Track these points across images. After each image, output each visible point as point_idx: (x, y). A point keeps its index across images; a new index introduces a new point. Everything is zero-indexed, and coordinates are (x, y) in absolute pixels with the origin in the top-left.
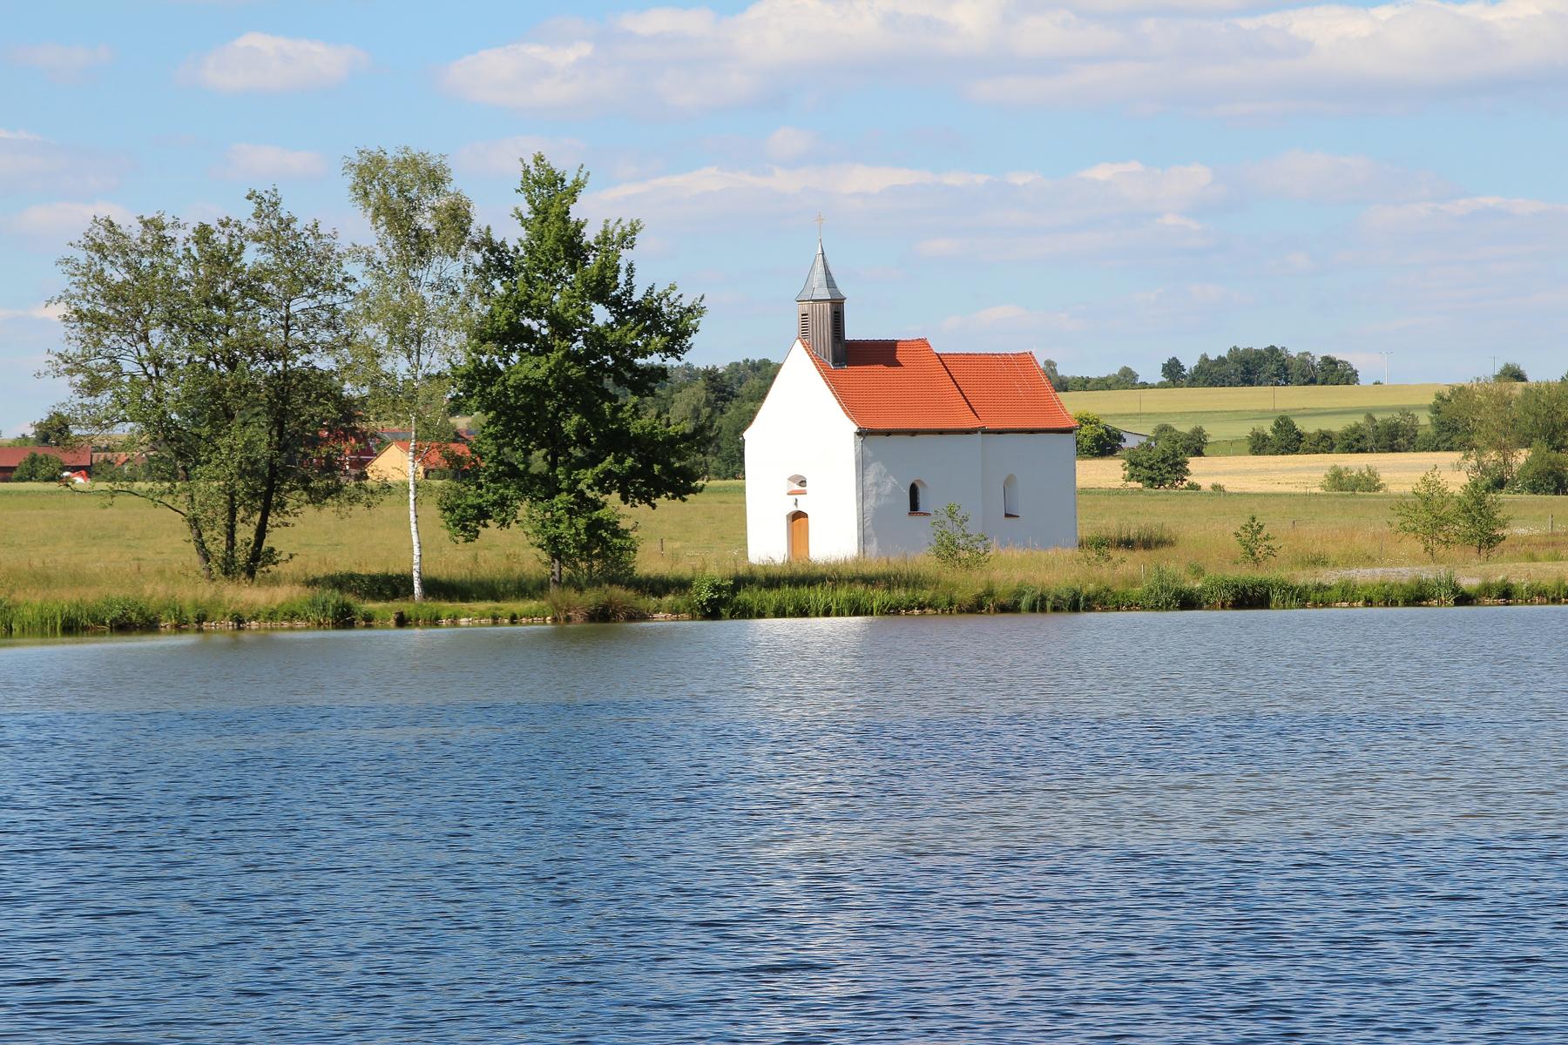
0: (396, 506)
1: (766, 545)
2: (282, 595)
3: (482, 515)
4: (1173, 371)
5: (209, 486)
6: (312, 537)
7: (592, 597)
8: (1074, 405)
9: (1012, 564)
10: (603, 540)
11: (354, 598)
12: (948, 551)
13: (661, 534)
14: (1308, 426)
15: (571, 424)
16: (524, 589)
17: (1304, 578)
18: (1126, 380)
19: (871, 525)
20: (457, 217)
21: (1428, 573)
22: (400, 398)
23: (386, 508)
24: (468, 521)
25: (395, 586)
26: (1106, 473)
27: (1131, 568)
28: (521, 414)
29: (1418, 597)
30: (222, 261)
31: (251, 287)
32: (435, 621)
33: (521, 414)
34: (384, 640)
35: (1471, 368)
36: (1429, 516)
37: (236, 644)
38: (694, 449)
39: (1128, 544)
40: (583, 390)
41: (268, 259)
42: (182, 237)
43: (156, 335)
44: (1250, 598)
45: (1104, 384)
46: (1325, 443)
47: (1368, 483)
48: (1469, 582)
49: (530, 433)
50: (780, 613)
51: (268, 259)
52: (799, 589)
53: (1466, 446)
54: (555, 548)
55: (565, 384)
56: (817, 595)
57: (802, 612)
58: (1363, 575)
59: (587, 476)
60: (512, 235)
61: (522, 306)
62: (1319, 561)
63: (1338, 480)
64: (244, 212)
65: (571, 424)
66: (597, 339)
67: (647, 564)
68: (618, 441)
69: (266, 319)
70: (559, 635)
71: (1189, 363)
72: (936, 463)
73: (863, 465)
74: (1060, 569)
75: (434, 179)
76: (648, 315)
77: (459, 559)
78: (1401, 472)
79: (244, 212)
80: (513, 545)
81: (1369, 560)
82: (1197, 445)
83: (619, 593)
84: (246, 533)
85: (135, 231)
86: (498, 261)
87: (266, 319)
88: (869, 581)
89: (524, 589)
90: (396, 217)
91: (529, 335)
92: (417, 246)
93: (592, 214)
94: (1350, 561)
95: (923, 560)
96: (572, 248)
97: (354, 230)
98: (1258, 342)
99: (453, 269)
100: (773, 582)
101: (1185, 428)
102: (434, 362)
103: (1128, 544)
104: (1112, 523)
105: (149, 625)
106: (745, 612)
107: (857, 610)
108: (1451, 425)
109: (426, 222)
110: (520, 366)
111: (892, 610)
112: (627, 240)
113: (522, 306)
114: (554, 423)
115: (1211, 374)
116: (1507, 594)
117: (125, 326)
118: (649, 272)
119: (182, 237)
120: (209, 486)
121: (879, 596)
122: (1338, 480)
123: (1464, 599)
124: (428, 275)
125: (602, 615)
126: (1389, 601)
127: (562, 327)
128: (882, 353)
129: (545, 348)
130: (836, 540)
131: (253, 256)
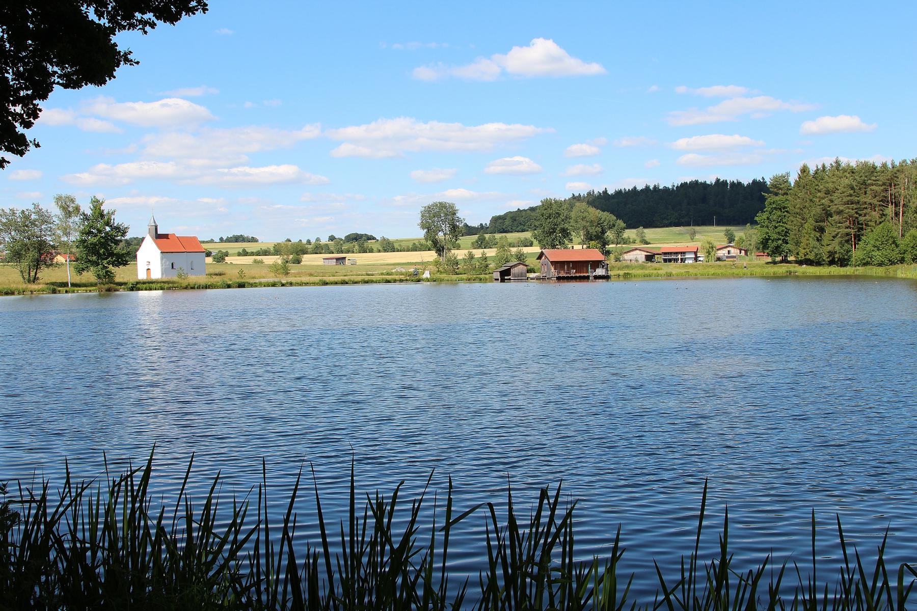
0: (63, 268)
1: (142, 276)
2: (41, 286)
3: (83, 270)
4: (221, 239)
5: (25, 264)
6: (46, 275)
7: (107, 286)
8: (205, 246)
9: (193, 279)
10: (109, 275)
11: (56, 287)
12: (180, 276)
13: (121, 274)
14: (249, 250)
15: (102, 251)
16: (92, 285)
17: (252, 281)
18: (212, 241)
19: (164, 272)
20: (77, 209)
21: (276, 280)
22: (64, 244)
23: (63, 268)
24: (80, 271)
25: (65, 285)
26: (209, 260)
27: (217, 279)
28: (92, 249)
29: (274, 285)
30: (27, 217)
31: (33, 223)
32: (73, 292)
33: (92, 249)
34: (64, 297)
35: (281, 239)
36: (274, 268)
37: (31, 298)
38: (126, 257)
39: (216, 275)
40: (104, 245)
41: (37, 217)
42: (18, 213)
43: (13, 233)
44: (241, 286)
45: (207, 242)
46: (252, 254)
47: (261, 262)
48: (284, 282)
49: (93, 253)
50: (146, 289)
51: (37, 217)
52: (149, 285)
53: (280, 254)
54: (99, 276)
55: (100, 243)
56: (154, 286)
57: (151, 289)
58: (263, 280)
59: (105, 262)
60: (89, 212)
61: (91, 227)
62: (254, 278)
63: (255, 261)
64: (31, 207)
65: (102, 251)
66: (107, 233)
67: (118, 279)
68: (112, 254)
69: (36, 230)
70: (100, 295)
71: (225, 238)
72: (174, 258)
73: (162, 259)
74: (203, 279)
75: (73, 201)
76: (117, 229)
77: (77, 279)
78: (269, 260)
79: (31, 207)
80: (90, 276)
81: (264, 278)
82: (227, 254)
83: (112, 285)
84: (33, 274)
85: (8, 211)
86: (86, 217)
87: (36, 230)
88: (164, 282)
89: (92, 285)
90: (64, 208)
91: (92, 233)
92: (68, 214)
93: (105, 208)
94: (260, 278)
95: (175, 279)
96: (102, 215)
97: (55, 211)
98: (360, 232)
99: (77, 219)
100: (144, 283)
101: (224, 251)
102: (72, 238)
103: (216, 275)
104: (212, 271)
105: (13, 293)
106: (139, 289)
107: (162, 289)
108: (277, 250)
109: (71, 209)
110: (91, 239)
111: (169, 289)
112: (113, 213)
113: (91, 227)
114: (98, 251)
115: (229, 240)
116: (291, 284)
117: (6, 231)
118: (117, 220)
119: (18, 213)
120: (25, 264)
121: (166, 286)
122: (255, 261)
123: (283, 285)
124: (71, 220)
125: (109, 290)
126: (268, 286)
127: (100, 231)
128: (166, 236)
129: (96, 236)
130: (156, 275)
131: (33, 217)
